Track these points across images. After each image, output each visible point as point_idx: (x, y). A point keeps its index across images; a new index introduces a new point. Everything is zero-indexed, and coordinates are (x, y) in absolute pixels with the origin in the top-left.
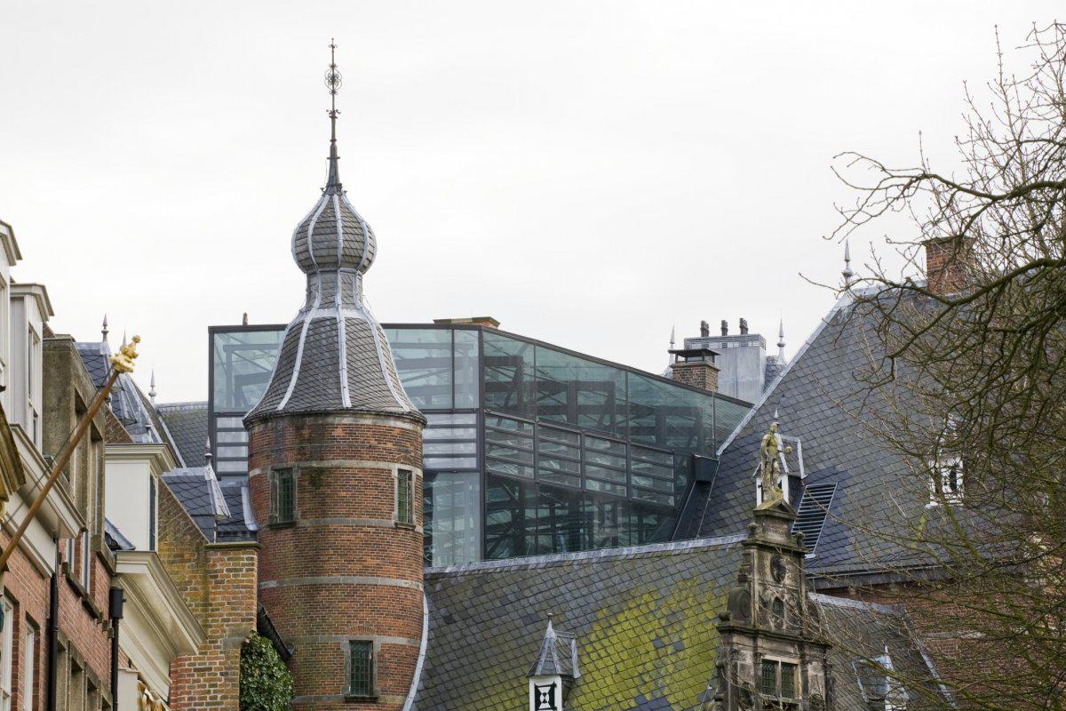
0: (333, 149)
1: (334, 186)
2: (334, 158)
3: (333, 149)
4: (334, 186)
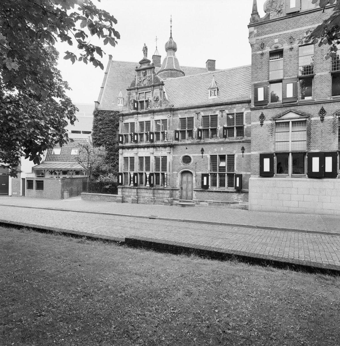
0: (171, 32)
1: (171, 37)
2: (171, 33)
3: (171, 32)
4: (171, 37)
